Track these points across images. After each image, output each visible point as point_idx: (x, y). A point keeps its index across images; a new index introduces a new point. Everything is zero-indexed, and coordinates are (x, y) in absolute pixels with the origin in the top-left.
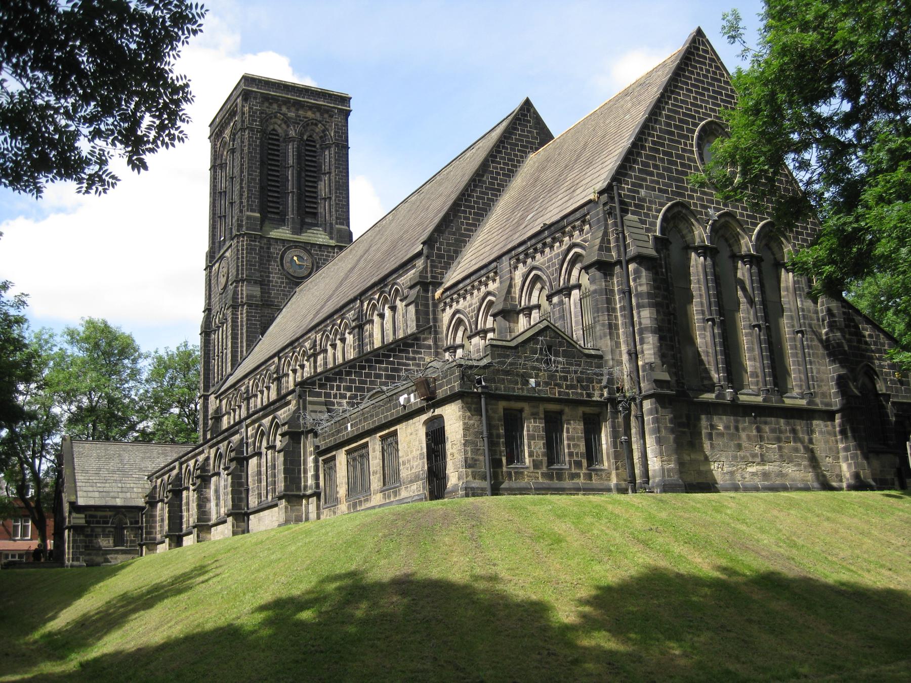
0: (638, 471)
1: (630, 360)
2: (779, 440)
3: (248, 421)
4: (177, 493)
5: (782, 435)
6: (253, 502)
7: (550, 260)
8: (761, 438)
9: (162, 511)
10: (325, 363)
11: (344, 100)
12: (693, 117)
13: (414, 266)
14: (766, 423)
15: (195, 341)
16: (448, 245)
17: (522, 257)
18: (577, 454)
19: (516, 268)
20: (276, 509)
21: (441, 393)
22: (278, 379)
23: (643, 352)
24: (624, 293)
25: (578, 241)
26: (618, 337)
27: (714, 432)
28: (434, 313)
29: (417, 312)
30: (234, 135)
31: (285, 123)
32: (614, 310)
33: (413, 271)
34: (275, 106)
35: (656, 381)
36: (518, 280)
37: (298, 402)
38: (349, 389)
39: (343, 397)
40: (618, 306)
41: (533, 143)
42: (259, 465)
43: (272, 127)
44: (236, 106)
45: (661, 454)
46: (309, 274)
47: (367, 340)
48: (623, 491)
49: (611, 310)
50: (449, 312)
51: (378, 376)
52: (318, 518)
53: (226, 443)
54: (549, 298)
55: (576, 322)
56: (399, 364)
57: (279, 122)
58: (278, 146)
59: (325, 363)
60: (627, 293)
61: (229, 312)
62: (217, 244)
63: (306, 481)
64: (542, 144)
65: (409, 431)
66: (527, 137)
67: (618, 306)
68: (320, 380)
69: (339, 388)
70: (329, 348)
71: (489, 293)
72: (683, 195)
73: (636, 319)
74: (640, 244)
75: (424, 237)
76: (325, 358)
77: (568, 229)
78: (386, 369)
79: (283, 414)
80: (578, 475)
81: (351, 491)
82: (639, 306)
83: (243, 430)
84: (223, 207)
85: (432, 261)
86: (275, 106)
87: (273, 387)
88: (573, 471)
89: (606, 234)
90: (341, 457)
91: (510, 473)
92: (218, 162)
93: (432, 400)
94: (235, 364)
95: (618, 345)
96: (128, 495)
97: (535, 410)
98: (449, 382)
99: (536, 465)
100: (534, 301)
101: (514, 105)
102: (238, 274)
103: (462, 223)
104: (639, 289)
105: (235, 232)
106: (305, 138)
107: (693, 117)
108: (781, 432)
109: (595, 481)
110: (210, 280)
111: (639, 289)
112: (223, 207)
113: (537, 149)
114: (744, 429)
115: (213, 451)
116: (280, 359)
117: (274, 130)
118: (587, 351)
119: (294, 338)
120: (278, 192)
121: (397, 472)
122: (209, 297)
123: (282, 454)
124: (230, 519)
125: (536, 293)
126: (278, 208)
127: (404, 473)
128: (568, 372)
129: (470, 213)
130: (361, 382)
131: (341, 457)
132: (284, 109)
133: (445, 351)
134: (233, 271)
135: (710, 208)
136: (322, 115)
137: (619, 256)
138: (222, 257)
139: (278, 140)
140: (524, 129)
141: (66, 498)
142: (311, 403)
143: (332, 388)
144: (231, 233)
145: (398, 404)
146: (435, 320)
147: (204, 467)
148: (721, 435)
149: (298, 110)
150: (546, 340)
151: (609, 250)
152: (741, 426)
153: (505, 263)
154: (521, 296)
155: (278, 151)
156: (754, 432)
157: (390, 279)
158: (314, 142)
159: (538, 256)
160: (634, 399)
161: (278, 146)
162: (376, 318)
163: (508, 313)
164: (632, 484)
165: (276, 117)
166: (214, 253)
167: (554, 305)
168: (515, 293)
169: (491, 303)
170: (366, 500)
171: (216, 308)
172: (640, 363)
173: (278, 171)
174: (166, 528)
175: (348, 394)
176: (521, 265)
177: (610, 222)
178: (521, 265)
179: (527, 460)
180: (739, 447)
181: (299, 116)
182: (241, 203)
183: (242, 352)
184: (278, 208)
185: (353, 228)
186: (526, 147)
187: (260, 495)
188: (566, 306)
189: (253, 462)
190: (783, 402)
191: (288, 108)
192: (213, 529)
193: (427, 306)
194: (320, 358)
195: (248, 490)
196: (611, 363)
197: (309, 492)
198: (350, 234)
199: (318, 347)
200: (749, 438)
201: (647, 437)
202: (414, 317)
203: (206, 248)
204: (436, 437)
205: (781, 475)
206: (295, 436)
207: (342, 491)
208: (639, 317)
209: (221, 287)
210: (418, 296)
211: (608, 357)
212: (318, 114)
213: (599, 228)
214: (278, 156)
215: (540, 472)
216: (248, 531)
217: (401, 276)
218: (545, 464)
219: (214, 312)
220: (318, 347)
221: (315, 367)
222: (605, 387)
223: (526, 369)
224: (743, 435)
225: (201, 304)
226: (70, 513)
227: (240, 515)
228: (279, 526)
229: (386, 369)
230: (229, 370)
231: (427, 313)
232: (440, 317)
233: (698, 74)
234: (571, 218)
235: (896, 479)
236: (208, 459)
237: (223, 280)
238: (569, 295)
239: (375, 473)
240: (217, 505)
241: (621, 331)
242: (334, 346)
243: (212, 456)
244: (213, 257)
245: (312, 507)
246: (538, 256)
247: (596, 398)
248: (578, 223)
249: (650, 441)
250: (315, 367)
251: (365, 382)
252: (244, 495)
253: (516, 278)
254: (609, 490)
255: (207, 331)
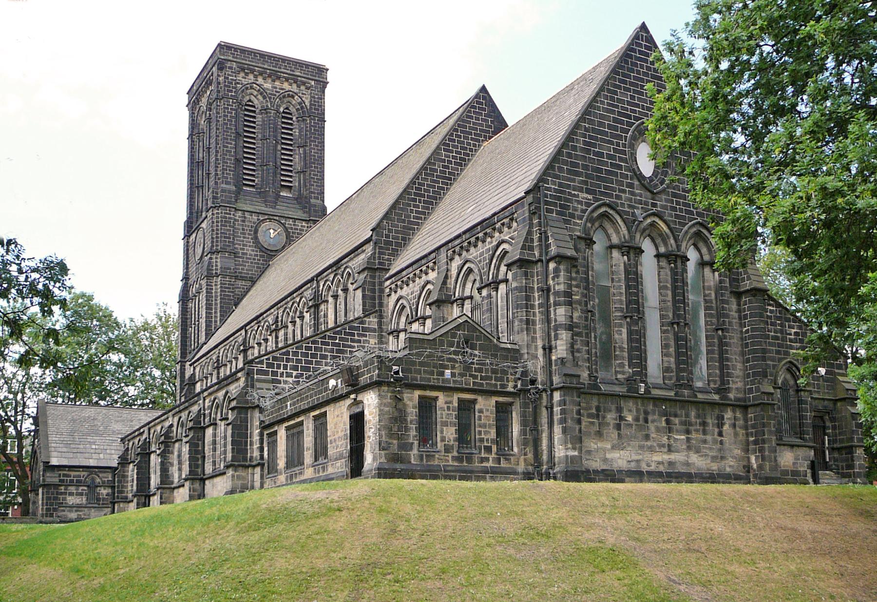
0: (545, 457)
1: (545, 355)
2: (688, 432)
3: (206, 394)
4: (145, 454)
5: (690, 428)
6: (209, 469)
7: (482, 254)
8: (670, 430)
9: (132, 471)
10: (286, 339)
11: (315, 76)
12: (629, 117)
13: (363, 251)
14: (676, 416)
15: (174, 310)
16: (397, 232)
17: (457, 249)
18: (487, 440)
19: (452, 259)
20: (225, 477)
21: (363, 380)
22: (245, 351)
23: (556, 347)
24: (543, 291)
25: (507, 238)
26: (535, 333)
27: (623, 423)
28: (380, 298)
29: (364, 296)
30: (211, 104)
31: (261, 94)
32: (533, 307)
33: (362, 256)
34: (251, 76)
35: (565, 375)
36: (454, 272)
37: (247, 379)
38: (295, 368)
39: (289, 375)
40: (537, 303)
41: (488, 132)
42: (214, 435)
43: (248, 98)
44: (212, 75)
45: (566, 443)
46: (284, 247)
47: (322, 320)
48: (528, 476)
49: (529, 306)
50: (394, 297)
51: (324, 357)
52: (262, 487)
53: (187, 412)
54: (480, 290)
55: (502, 315)
56: (344, 346)
57: (255, 93)
58: (254, 117)
59: (286, 339)
60: (546, 291)
61: (204, 282)
62: (195, 214)
63: (252, 452)
64: (495, 133)
65: (336, 413)
66: (482, 125)
67: (537, 303)
68: (268, 359)
69: (285, 367)
70: (290, 325)
71: (428, 282)
72: (611, 196)
73: (552, 316)
74: (562, 244)
75: (373, 224)
76: (286, 334)
77: (498, 225)
78: (332, 351)
79: (234, 389)
80: (487, 459)
81: (289, 465)
82: (556, 304)
83: (201, 402)
84: (200, 177)
85: (380, 248)
86: (251, 76)
87: (241, 358)
88: (483, 455)
89: (529, 233)
90: (282, 433)
91: (422, 456)
92: (196, 131)
93: (355, 386)
94: (209, 335)
95: (534, 339)
96: (102, 456)
97: (449, 399)
98: (369, 371)
99: (448, 449)
100: (467, 293)
101: (639, 24)
102: (212, 246)
103: (412, 211)
104: (557, 287)
105: (210, 204)
106: (282, 110)
107: (629, 117)
108: (690, 424)
109: (504, 464)
110: (188, 250)
111: (557, 287)
112: (200, 177)
113: (490, 138)
114: (653, 421)
115: (176, 419)
116: (246, 331)
117: (250, 101)
118: (503, 346)
119: (258, 313)
120: (253, 165)
121: (326, 449)
122: (187, 266)
123: (230, 427)
124: (187, 484)
125: (469, 285)
126: (254, 181)
127: (331, 452)
128: (484, 364)
129: (420, 202)
130: (307, 362)
131: (282, 433)
132: (260, 80)
133: (389, 334)
134: (209, 244)
135: (638, 208)
136: (298, 86)
137: (541, 255)
138: (198, 228)
139: (254, 112)
140: (480, 117)
141: (42, 458)
142: (258, 380)
143: (279, 367)
144: (207, 204)
145: (327, 389)
146: (381, 305)
147: (167, 435)
148: (630, 425)
149: (274, 81)
150: (464, 334)
151: (531, 248)
152: (650, 418)
153: (443, 257)
154: (455, 288)
155: (254, 122)
156: (664, 424)
157: (343, 262)
158: (291, 114)
159: (472, 249)
160: (545, 390)
161: (254, 117)
162: (331, 300)
163: (443, 301)
164: (538, 471)
165: (252, 88)
166: (192, 223)
167: (483, 298)
168: (450, 284)
169: (429, 292)
170: (301, 473)
171: (193, 278)
172: (554, 358)
173: (254, 144)
174: (135, 488)
175: (295, 373)
176: (457, 257)
177: (536, 221)
178: (457, 257)
179: (439, 445)
180: (647, 437)
181: (276, 88)
182: (216, 174)
183: (216, 322)
184: (254, 181)
185: (327, 203)
186: (480, 136)
187: (214, 463)
188: (494, 300)
189: (209, 432)
190: (696, 396)
191: (264, 79)
192: (176, 491)
193: (373, 291)
194: (281, 333)
195: (204, 457)
196: (526, 356)
197: (254, 463)
198: (324, 209)
199: (280, 324)
200: (658, 430)
201: (555, 427)
202: (361, 301)
203: (183, 216)
204: (357, 421)
205: (688, 464)
206: (244, 407)
207: (281, 463)
208: (555, 314)
209: (198, 257)
210: (365, 282)
211: (524, 351)
212: (295, 86)
213: (525, 226)
214: (254, 128)
215: (450, 455)
216: (204, 496)
217: (351, 259)
218: (455, 449)
219: (191, 281)
220: (280, 324)
221: (277, 343)
222: (519, 379)
223: (443, 360)
224: (652, 427)
225: (180, 273)
226: (44, 471)
227: (198, 479)
228: (226, 493)
229: (332, 351)
230: (203, 339)
231: (374, 298)
232: (385, 302)
233: (638, 72)
234: (501, 215)
235: (809, 471)
236: (171, 426)
237: (199, 251)
238: (497, 289)
239: (308, 449)
240: (180, 469)
241: (538, 327)
242: (294, 323)
243: (175, 424)
244: (191, 227)
245: (257, 477)
246: (472, 249)
247: (510, 389)
248: (506, 221)
249: (557, 429)
250: (277, 343)
251: (311, 363)
252: (200, 462)
253: (453, 269)
254: (515, 473)
255: (185, 298)
